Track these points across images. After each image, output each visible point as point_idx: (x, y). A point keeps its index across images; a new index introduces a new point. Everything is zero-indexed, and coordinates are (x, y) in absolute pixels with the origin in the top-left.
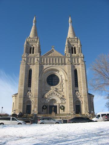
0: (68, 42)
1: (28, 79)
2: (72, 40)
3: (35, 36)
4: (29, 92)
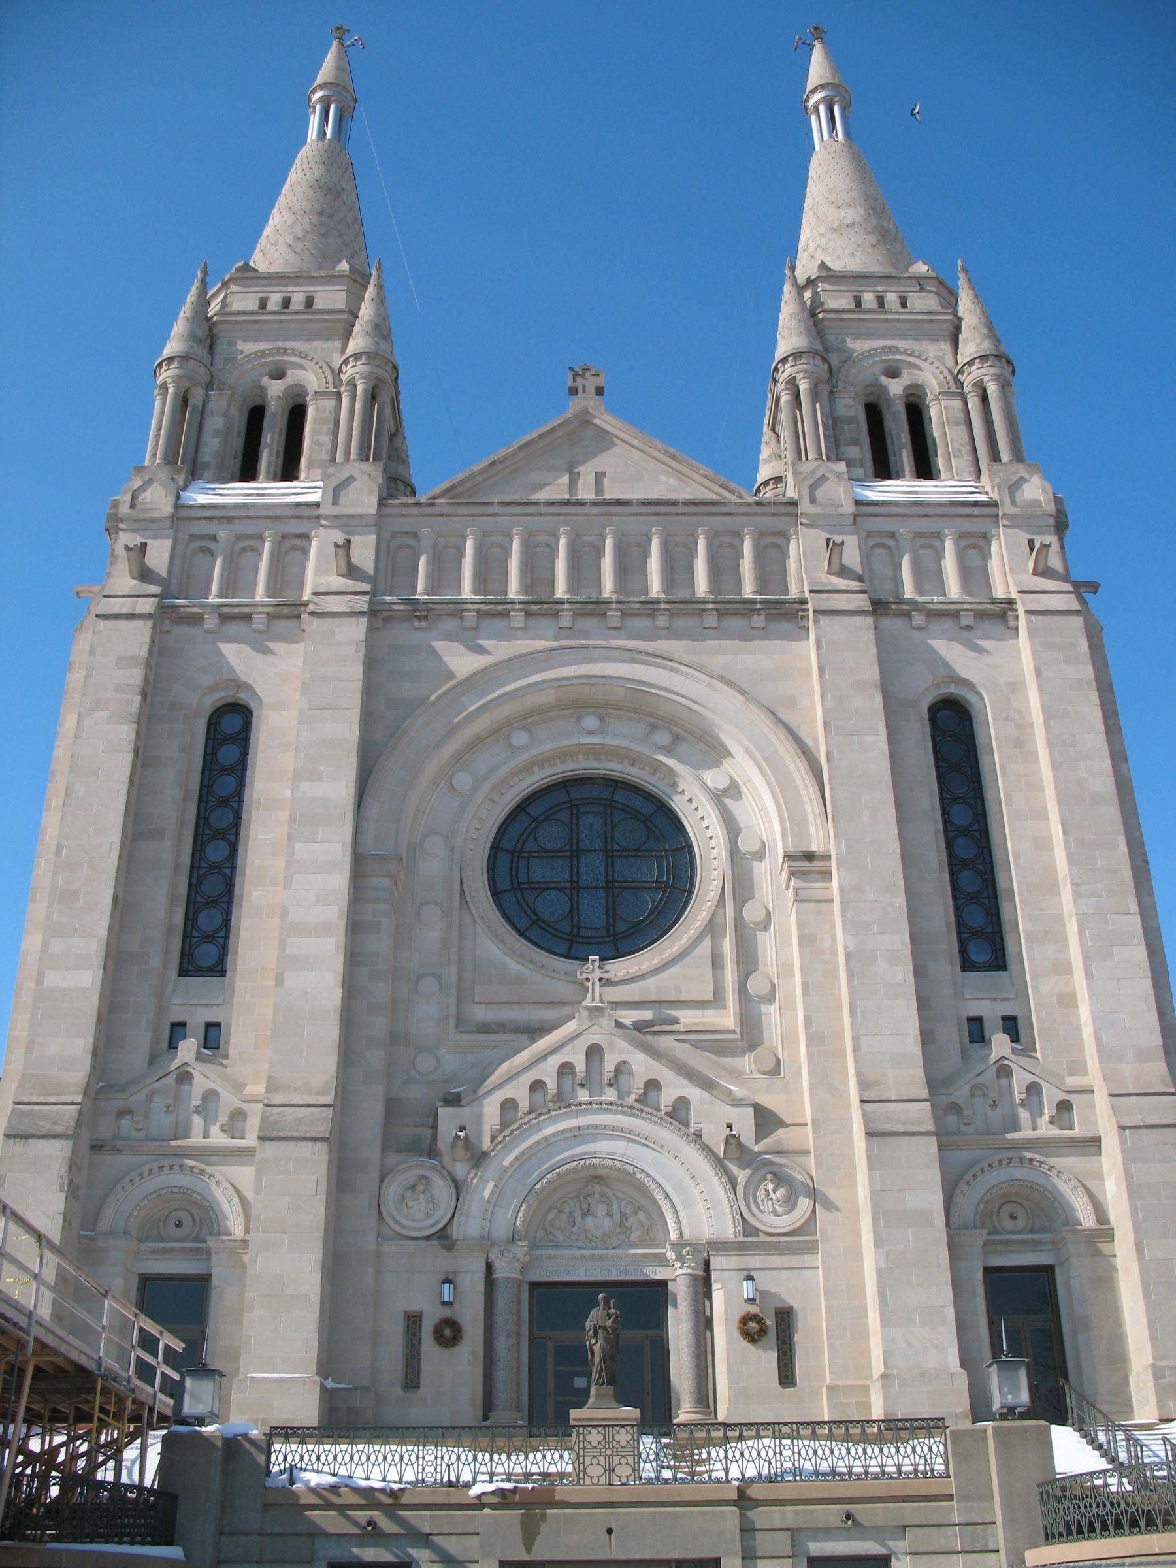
0: (813, 316)
2: (869, 299)
3: (326, 258)
4: (188, 1048)
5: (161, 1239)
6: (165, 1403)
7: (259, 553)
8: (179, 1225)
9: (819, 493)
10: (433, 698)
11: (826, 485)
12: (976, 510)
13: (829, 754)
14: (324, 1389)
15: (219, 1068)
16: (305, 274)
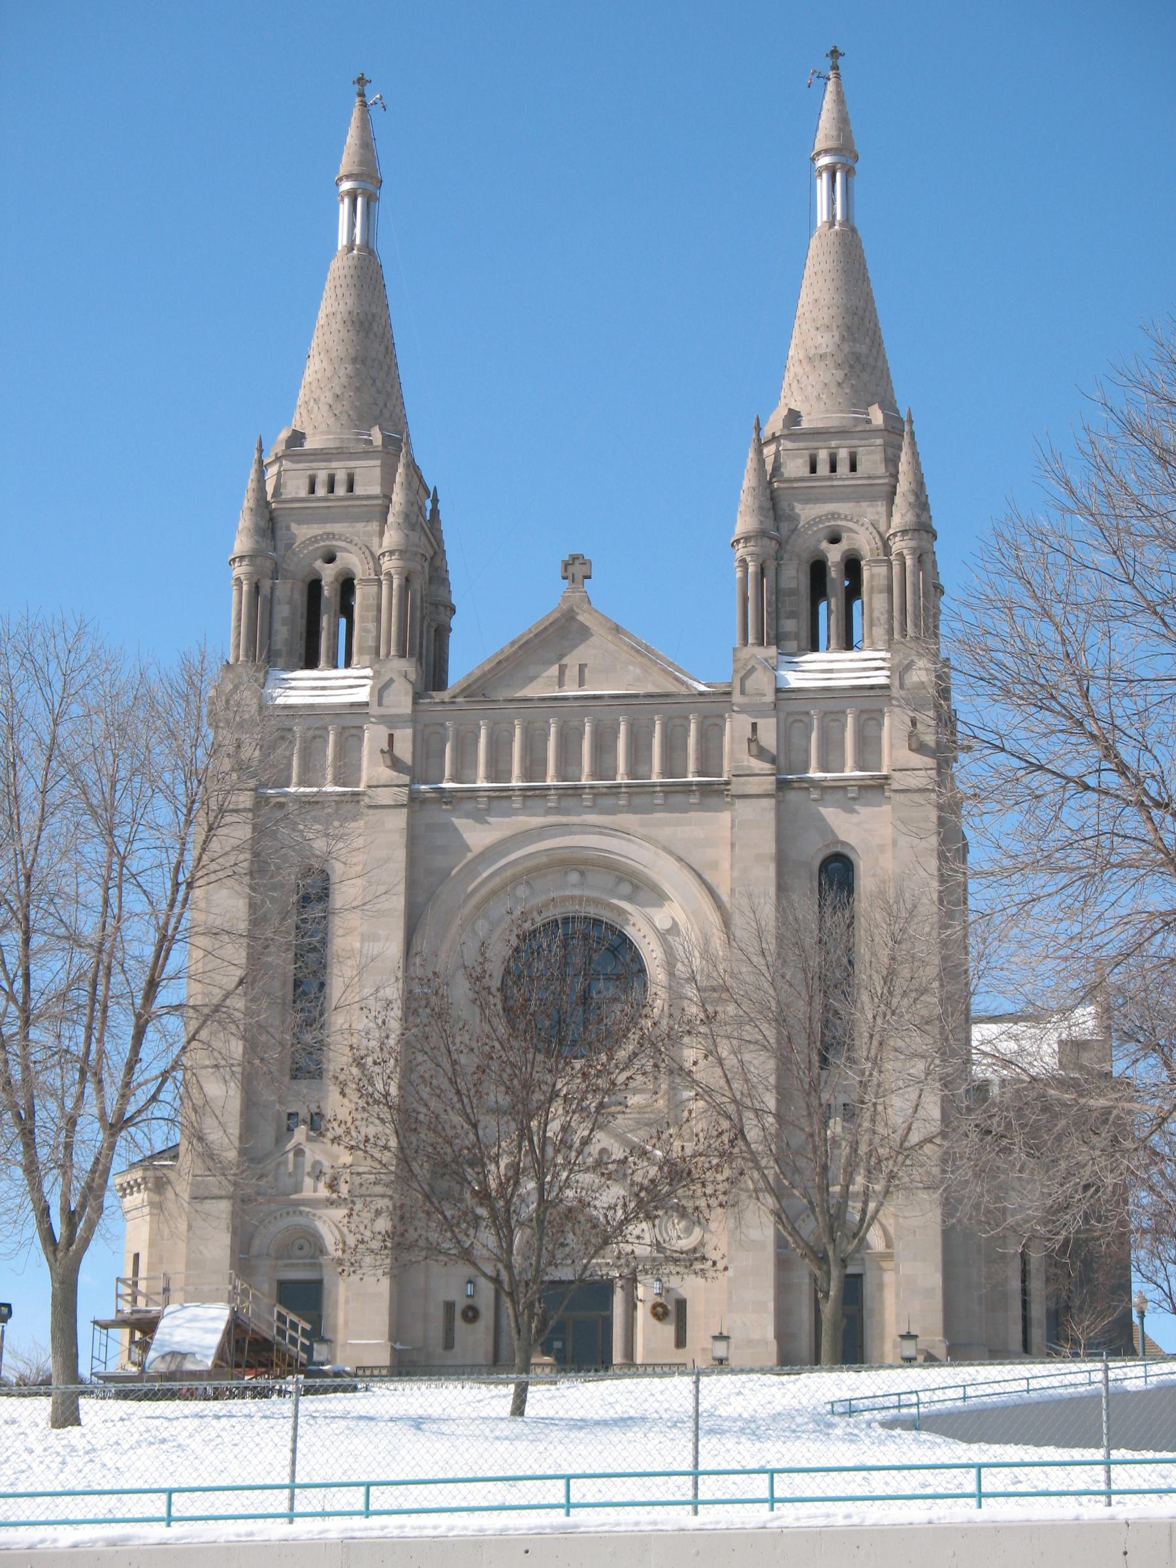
1: (813, 1339)
5: (290, 1257)
6: (303, 1356)
7: (327, 742)
8: (301, 1248)
9: (748, 683)
10: (454, 872)
11: (754, 675)
12: (872, 693)
13: (346, 1322)
14: (393, 1349)
15: (321, 1145)
16: (345, 451)
